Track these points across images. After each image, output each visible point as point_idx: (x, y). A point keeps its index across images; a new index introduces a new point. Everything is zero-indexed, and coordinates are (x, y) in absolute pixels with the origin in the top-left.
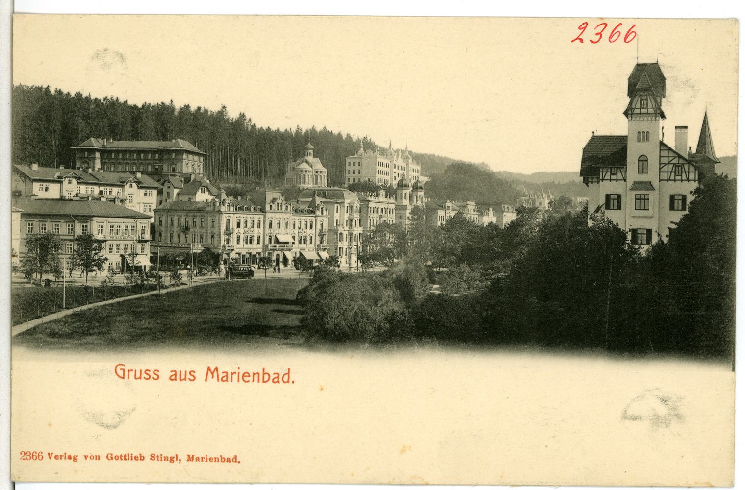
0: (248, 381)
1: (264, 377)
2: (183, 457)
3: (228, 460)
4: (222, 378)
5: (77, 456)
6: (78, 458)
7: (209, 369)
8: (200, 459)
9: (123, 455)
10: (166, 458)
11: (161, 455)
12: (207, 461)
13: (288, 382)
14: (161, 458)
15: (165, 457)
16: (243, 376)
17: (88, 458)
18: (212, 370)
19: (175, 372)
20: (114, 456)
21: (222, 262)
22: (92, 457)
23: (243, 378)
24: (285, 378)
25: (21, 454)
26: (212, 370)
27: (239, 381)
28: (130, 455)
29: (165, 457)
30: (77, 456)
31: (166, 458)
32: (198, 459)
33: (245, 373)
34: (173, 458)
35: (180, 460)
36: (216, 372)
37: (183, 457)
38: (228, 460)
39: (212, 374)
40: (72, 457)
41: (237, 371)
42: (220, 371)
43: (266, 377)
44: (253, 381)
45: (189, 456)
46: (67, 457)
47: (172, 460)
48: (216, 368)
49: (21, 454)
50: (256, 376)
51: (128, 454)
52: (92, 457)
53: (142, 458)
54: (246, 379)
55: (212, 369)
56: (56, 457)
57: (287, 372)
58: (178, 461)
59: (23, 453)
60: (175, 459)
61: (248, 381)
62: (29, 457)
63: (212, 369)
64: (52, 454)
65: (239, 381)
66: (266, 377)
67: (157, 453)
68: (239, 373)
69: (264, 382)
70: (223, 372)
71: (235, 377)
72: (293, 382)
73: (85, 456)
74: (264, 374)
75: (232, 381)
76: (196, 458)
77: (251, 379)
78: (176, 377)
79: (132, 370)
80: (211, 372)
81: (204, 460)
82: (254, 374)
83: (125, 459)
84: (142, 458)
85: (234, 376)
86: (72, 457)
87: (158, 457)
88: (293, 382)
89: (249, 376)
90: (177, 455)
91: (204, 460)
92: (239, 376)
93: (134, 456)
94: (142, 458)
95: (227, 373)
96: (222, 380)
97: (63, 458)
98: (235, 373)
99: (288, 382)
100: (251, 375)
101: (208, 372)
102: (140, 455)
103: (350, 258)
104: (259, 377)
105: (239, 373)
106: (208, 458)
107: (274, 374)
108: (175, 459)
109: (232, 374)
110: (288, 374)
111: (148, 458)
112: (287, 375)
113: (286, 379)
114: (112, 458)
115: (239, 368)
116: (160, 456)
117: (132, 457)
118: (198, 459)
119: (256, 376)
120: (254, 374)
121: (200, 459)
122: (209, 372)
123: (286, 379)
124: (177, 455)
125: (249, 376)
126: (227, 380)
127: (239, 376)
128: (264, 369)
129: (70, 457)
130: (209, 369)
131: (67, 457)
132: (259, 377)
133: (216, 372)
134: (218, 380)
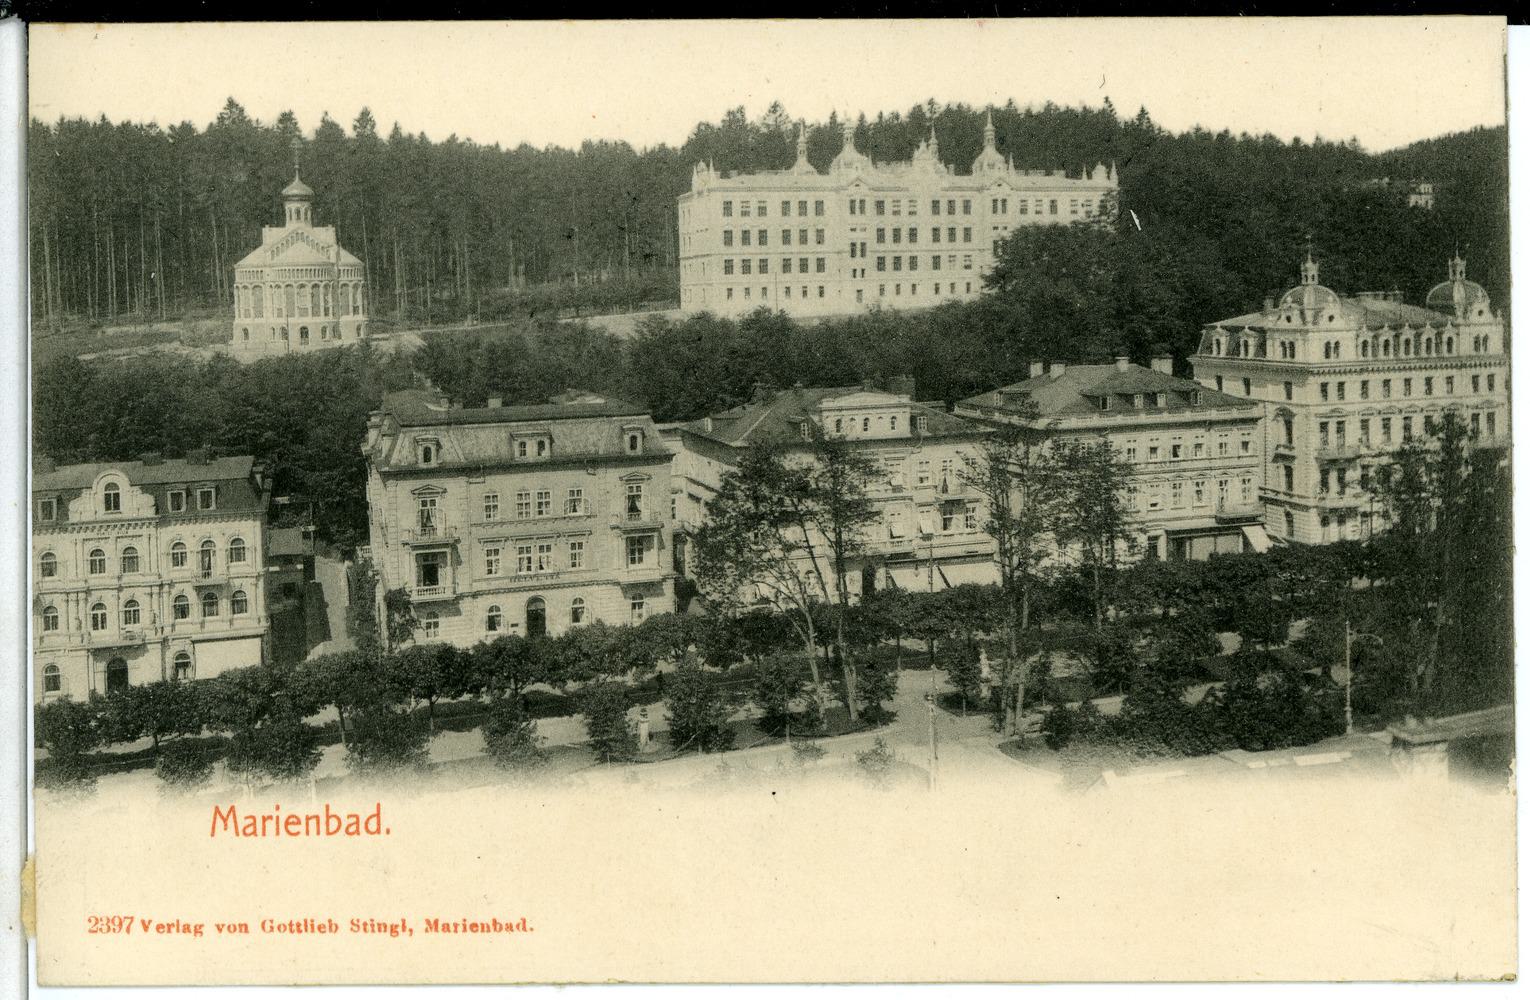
0: (298, 833)
1: (327, 823)
2: (416, 922)
3: (510, 927)
4: (245, 828)
5: (201, 926)
6: (203, 929)
7: (217, 811)
8: (452, 928)
9: (294, 923)
10: (382, 927)
11: (372, 920)
12: (465, 930)
13: (378, 831)
14: (372, 926)
15: (379, 925)
16: (287, 823)
17: (225, 930)
18: (225, 814)
19: (254, 818)
20: (275, 925)
21: (406, 645)
22: (232, 928)
23: (286, 828)
24: (372, 824)
25: (90, 921)
26: (225, 814)
27: (278, 833)
28: (309, 922)
29: (379, 925)
30: (201, 926)
31: (382, 927)
32: (446, 928)
33: (289, 817)
34: (397, 926)
35: (411, 930)
36: (231, 817)
37: (416, 922)
38: (510, 927)
39: (225, 820)
40: (192, 929)
41: (275, 814)
42: (241, 814)
43: (334, 823)
44: (307, 833)
45: (428, 922)
46: (181, 928)
47: (394, 930)
48: (232, 809)
49: (90, 921)
50: (313, 823)
51: (306, 921)
52: (232, 928)
53: (334, 927)
54: (292, 828)
55: (224, 811)
56: (159, 927)
57: (375, 812)
58: (408, 932)
59: (93, 920)
60: (400, 929)
61: (298, 833)
62: (105, 928)
63: (224, 811)
64: (150, 922)
65: (278, 833)
66: (334, 823)
67: (238, 937)
68: (278, 818)
69: (329, 833)
70: (247, 818)
71: (271, 825)
72: (388, 832)
73: (218, 926)
74: (328, 817)
75: (264, 834)
76: (443, 925)
77: (302, 828)
78: (358, 828)
79: (270, 817)
80: (222, 817)
81: (460, 928)
82: (308, 819)
83: (300, 931)
84: (333, 927)
85: (268, 823)
86: (192, 929)
87: (365, 924)
88: (388, 832)
89: (299, 822)
90: (404, 921)
91: (460, 928)
92: (277, 823)
93: (316, 925)
94: (334, 927)
95: (357, 817)
96: (245, 834)
97: (174, 930)
98: (270, 817)
99: (378, 831)
100: (303, 822)
101: (215, 819)
102: (330, 921)
103: (141, 343)
104: (318, 823)
105: (278, 818)
106: (468, 924)
107: (247, 818)
108: (400, 929)
109: (264, 819)
110: (378, 815)
111: (345, 926)
112: (374, 820)
113: (373, 826)
114: (272, 928)
115: (278, 808)
116: (369, 923)
117: (312, 926)
118: (446, 928)
119: (313, 823)
120: (308, 819)
121: (452, 928)
122: (219, 819)
123: (373, 826)
124: (404, 921)
125: (299, 822)
126: (254, 833)
127: (277, 823)
128: (327, 807)
129: (187, 929)
130: (217, 811)
131: (181, 928)
132: (318, 823)
133: (231, 817)
134: (237, 834)
